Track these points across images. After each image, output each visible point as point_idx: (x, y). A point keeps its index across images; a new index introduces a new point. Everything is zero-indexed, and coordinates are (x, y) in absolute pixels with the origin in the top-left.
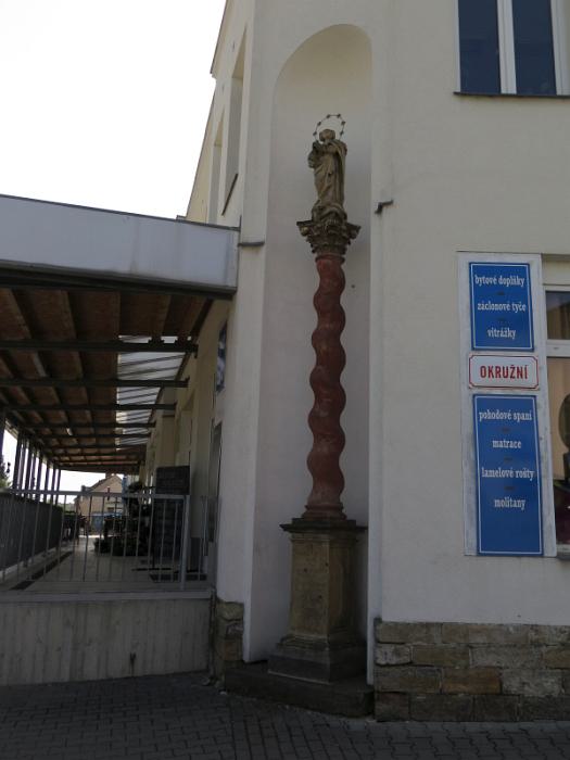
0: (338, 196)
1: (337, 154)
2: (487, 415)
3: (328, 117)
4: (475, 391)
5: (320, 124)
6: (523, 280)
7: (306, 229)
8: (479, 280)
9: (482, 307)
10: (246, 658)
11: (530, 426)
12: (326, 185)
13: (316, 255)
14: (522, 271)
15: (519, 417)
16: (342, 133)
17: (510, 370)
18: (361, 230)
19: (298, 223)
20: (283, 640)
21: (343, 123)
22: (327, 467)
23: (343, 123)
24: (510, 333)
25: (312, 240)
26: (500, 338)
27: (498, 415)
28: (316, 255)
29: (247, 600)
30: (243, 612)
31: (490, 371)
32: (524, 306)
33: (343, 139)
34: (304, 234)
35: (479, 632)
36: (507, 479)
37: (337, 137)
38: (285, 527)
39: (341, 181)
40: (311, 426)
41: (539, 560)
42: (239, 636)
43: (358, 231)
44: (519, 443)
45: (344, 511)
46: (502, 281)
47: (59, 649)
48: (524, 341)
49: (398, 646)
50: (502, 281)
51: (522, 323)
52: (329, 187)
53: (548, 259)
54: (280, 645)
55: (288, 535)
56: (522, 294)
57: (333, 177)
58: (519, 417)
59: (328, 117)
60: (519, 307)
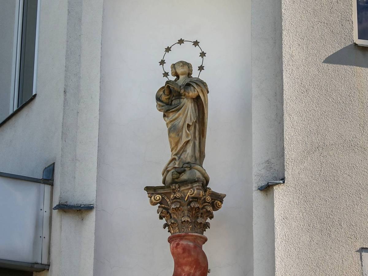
0: (197, 154)
1: (198, 97)
3: (181, 42)
5: (168, 49)
7: (158, 197)
12: (184, 139)
13: (164, 221)
16: (201, 68)
19: (147, 189)
21: (203, 54)
23: (203, 54)
24: (281, 182)
25: (165, 213)
28: (164, 221)
33: (203, 76)
34: (149, 197)
35: (98, 173)
37: (195, 74)
39: (202, 133)
52: (188, 142)
57: (192, 128)
59: (181, 42)
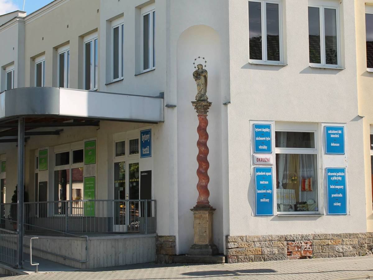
2: (259, 174)
3: (199, 57)
4: (255, 166)
6: (271, 191)
8: (256, 130)
9: (257, 139)
10: (177, 253)
11: (270, 177)
14: (269, 127)
15: (267, 174)
16: (205, 66)
17: (265, 159)
18: (212, 104)
19: (192, 102)
20: (192, 246)
22: (203, 189)
23: (206, 62)
24: (265, 147)
26: (262, 149)
27: (262, 174)
29: (177, 235)
30: (175, 239)
31: (260, 160)
32: (270, 138)
36: (264, 193)
38: (192, 210)
40: (198, 175)
41: (276, 120)
42: (175, 246)
43: (211, 104)
44: (268, 182)
45: (209, 204)
46: (264, 130)
47: (111, 256)
48: (269, 151)
49: (234, 243)
50: (264, 130)
51: (268, 143)
52: (202, 89)
53: (277, 122)
54: (192, 248)
55: (192, 212)
56: (268, 134)
58: (267, 174)
59: (199, 57)
60: (268, 139)
